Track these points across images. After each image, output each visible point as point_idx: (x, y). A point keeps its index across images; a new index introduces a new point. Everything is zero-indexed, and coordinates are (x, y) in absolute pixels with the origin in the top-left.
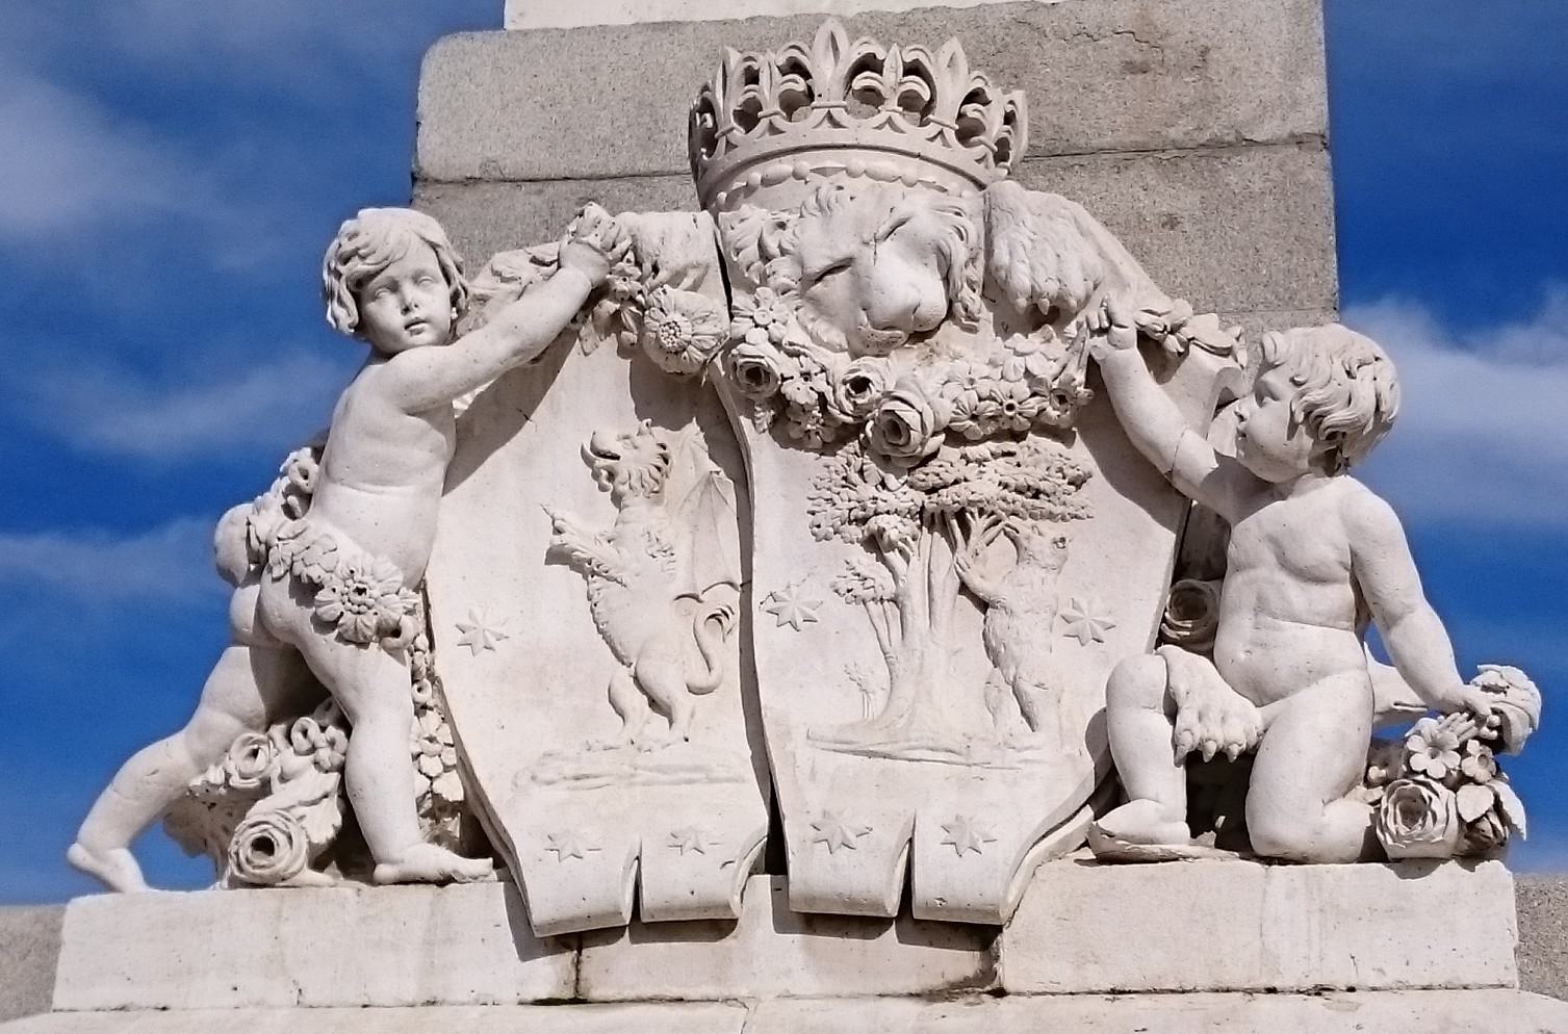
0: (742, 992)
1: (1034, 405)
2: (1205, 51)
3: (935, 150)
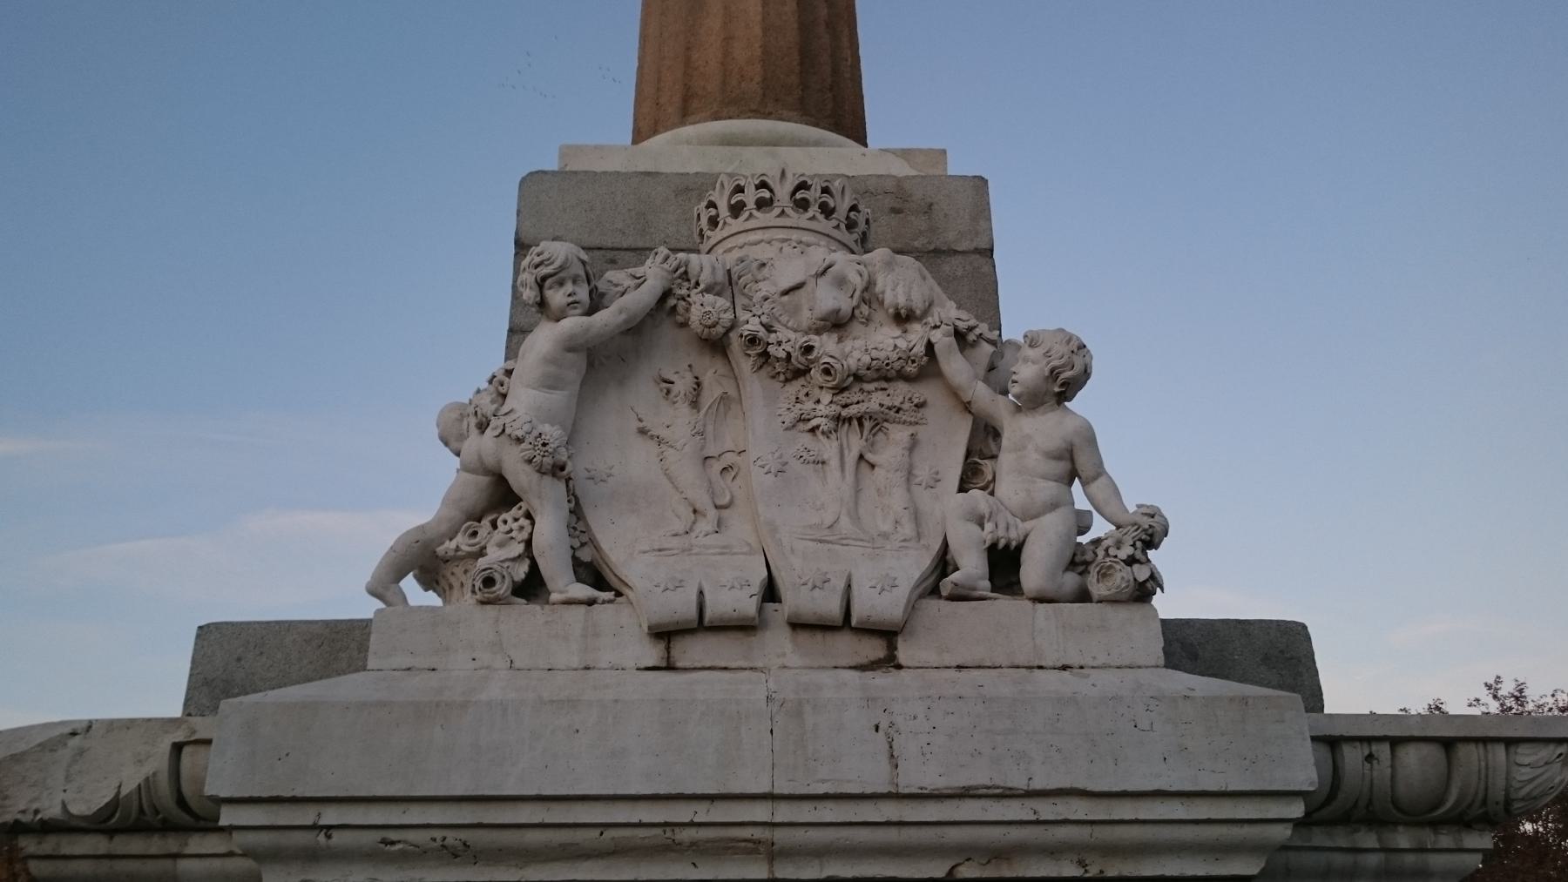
0: (760, 665)
2: (931, 205)
3: (835, 233)
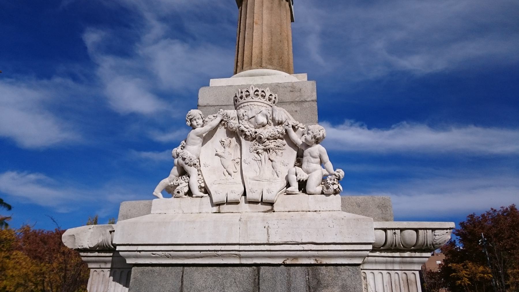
3: (266, 102)
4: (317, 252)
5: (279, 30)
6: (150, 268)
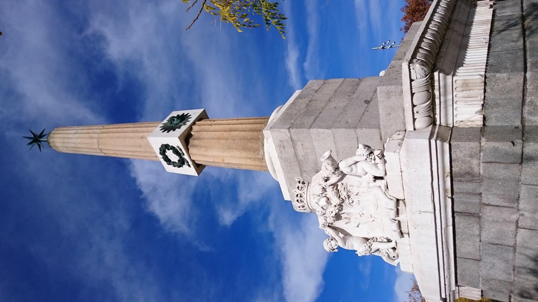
1: (335, 190)
4: (444, 253)
5: (224, 141)
6: (458, 276)
